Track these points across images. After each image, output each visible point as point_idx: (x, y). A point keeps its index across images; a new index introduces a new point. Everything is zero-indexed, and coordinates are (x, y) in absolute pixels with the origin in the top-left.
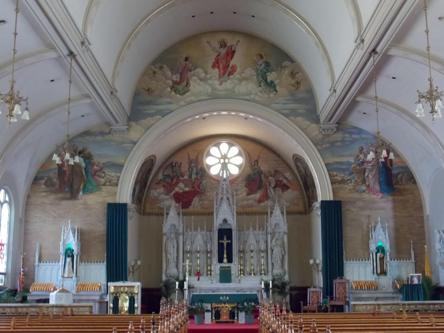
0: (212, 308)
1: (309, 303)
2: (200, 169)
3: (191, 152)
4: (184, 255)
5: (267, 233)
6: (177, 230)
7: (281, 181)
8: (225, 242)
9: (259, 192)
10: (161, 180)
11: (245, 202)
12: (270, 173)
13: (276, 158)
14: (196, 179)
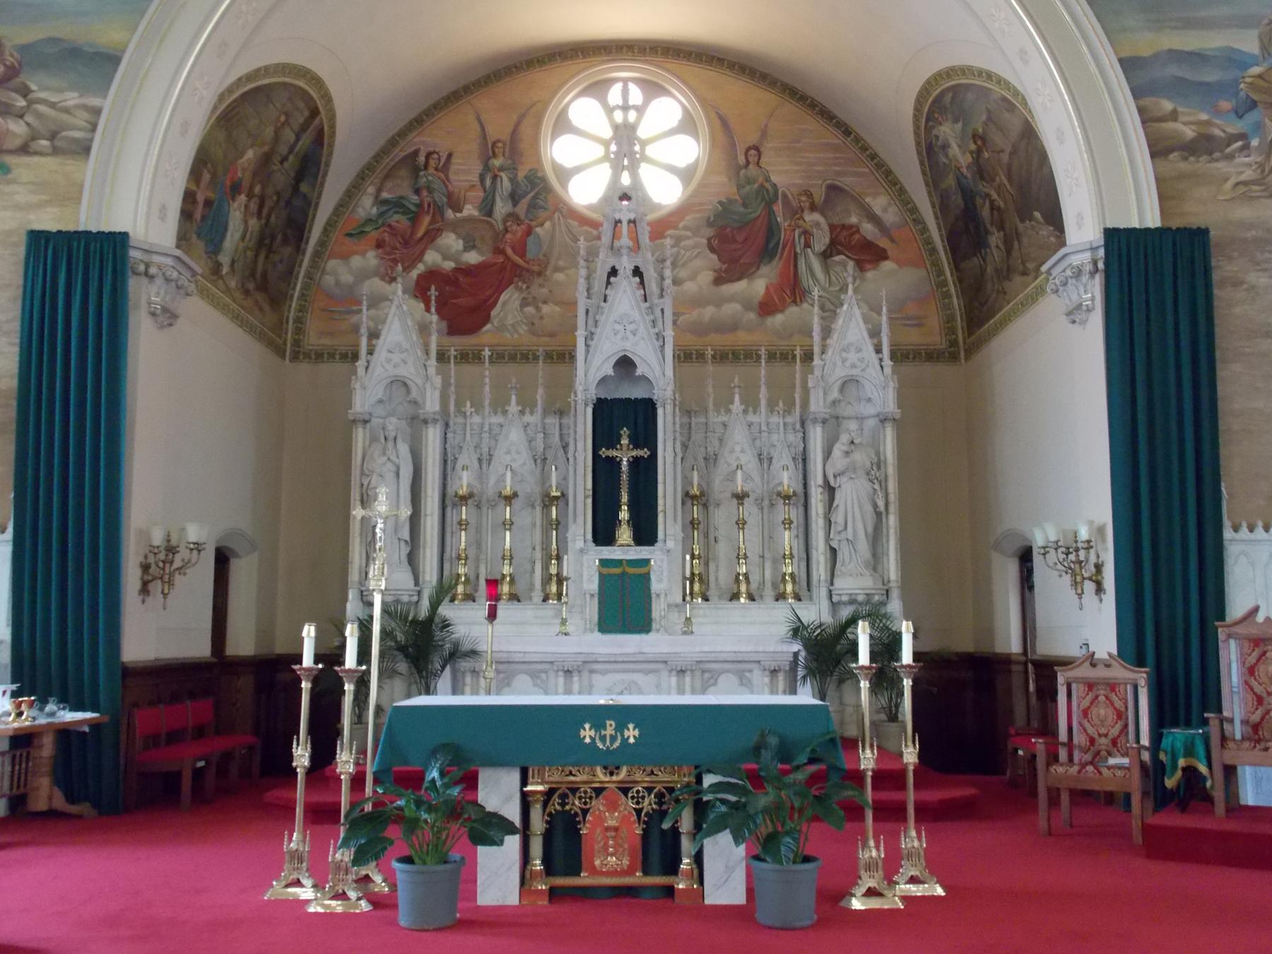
0: (526, 801)
1: (1070, 745)
2: (526, 177)
3: (492, 113)
4: (449, 510)
5: (803, 424)
6: (415, 403)
7: (854, 229)
8: (625, 455)
9: (764, 269)
10: (369, 221)
11: (709, 312)
12: (810, 195)
13: (833, 137)
14: (512, 216)
